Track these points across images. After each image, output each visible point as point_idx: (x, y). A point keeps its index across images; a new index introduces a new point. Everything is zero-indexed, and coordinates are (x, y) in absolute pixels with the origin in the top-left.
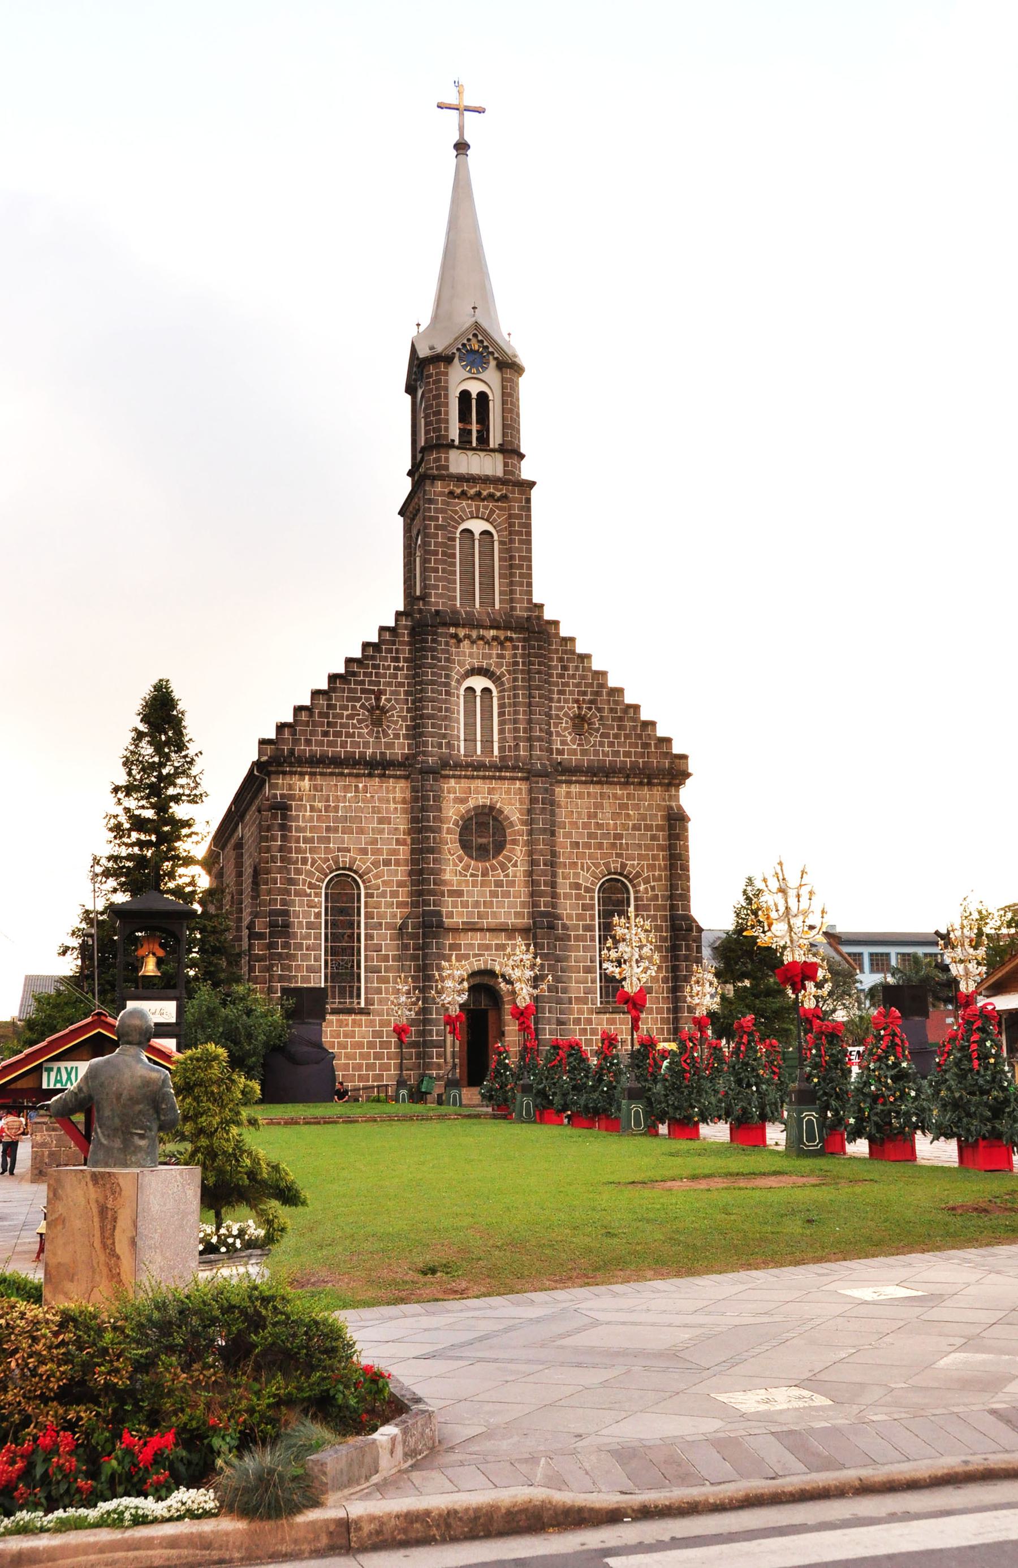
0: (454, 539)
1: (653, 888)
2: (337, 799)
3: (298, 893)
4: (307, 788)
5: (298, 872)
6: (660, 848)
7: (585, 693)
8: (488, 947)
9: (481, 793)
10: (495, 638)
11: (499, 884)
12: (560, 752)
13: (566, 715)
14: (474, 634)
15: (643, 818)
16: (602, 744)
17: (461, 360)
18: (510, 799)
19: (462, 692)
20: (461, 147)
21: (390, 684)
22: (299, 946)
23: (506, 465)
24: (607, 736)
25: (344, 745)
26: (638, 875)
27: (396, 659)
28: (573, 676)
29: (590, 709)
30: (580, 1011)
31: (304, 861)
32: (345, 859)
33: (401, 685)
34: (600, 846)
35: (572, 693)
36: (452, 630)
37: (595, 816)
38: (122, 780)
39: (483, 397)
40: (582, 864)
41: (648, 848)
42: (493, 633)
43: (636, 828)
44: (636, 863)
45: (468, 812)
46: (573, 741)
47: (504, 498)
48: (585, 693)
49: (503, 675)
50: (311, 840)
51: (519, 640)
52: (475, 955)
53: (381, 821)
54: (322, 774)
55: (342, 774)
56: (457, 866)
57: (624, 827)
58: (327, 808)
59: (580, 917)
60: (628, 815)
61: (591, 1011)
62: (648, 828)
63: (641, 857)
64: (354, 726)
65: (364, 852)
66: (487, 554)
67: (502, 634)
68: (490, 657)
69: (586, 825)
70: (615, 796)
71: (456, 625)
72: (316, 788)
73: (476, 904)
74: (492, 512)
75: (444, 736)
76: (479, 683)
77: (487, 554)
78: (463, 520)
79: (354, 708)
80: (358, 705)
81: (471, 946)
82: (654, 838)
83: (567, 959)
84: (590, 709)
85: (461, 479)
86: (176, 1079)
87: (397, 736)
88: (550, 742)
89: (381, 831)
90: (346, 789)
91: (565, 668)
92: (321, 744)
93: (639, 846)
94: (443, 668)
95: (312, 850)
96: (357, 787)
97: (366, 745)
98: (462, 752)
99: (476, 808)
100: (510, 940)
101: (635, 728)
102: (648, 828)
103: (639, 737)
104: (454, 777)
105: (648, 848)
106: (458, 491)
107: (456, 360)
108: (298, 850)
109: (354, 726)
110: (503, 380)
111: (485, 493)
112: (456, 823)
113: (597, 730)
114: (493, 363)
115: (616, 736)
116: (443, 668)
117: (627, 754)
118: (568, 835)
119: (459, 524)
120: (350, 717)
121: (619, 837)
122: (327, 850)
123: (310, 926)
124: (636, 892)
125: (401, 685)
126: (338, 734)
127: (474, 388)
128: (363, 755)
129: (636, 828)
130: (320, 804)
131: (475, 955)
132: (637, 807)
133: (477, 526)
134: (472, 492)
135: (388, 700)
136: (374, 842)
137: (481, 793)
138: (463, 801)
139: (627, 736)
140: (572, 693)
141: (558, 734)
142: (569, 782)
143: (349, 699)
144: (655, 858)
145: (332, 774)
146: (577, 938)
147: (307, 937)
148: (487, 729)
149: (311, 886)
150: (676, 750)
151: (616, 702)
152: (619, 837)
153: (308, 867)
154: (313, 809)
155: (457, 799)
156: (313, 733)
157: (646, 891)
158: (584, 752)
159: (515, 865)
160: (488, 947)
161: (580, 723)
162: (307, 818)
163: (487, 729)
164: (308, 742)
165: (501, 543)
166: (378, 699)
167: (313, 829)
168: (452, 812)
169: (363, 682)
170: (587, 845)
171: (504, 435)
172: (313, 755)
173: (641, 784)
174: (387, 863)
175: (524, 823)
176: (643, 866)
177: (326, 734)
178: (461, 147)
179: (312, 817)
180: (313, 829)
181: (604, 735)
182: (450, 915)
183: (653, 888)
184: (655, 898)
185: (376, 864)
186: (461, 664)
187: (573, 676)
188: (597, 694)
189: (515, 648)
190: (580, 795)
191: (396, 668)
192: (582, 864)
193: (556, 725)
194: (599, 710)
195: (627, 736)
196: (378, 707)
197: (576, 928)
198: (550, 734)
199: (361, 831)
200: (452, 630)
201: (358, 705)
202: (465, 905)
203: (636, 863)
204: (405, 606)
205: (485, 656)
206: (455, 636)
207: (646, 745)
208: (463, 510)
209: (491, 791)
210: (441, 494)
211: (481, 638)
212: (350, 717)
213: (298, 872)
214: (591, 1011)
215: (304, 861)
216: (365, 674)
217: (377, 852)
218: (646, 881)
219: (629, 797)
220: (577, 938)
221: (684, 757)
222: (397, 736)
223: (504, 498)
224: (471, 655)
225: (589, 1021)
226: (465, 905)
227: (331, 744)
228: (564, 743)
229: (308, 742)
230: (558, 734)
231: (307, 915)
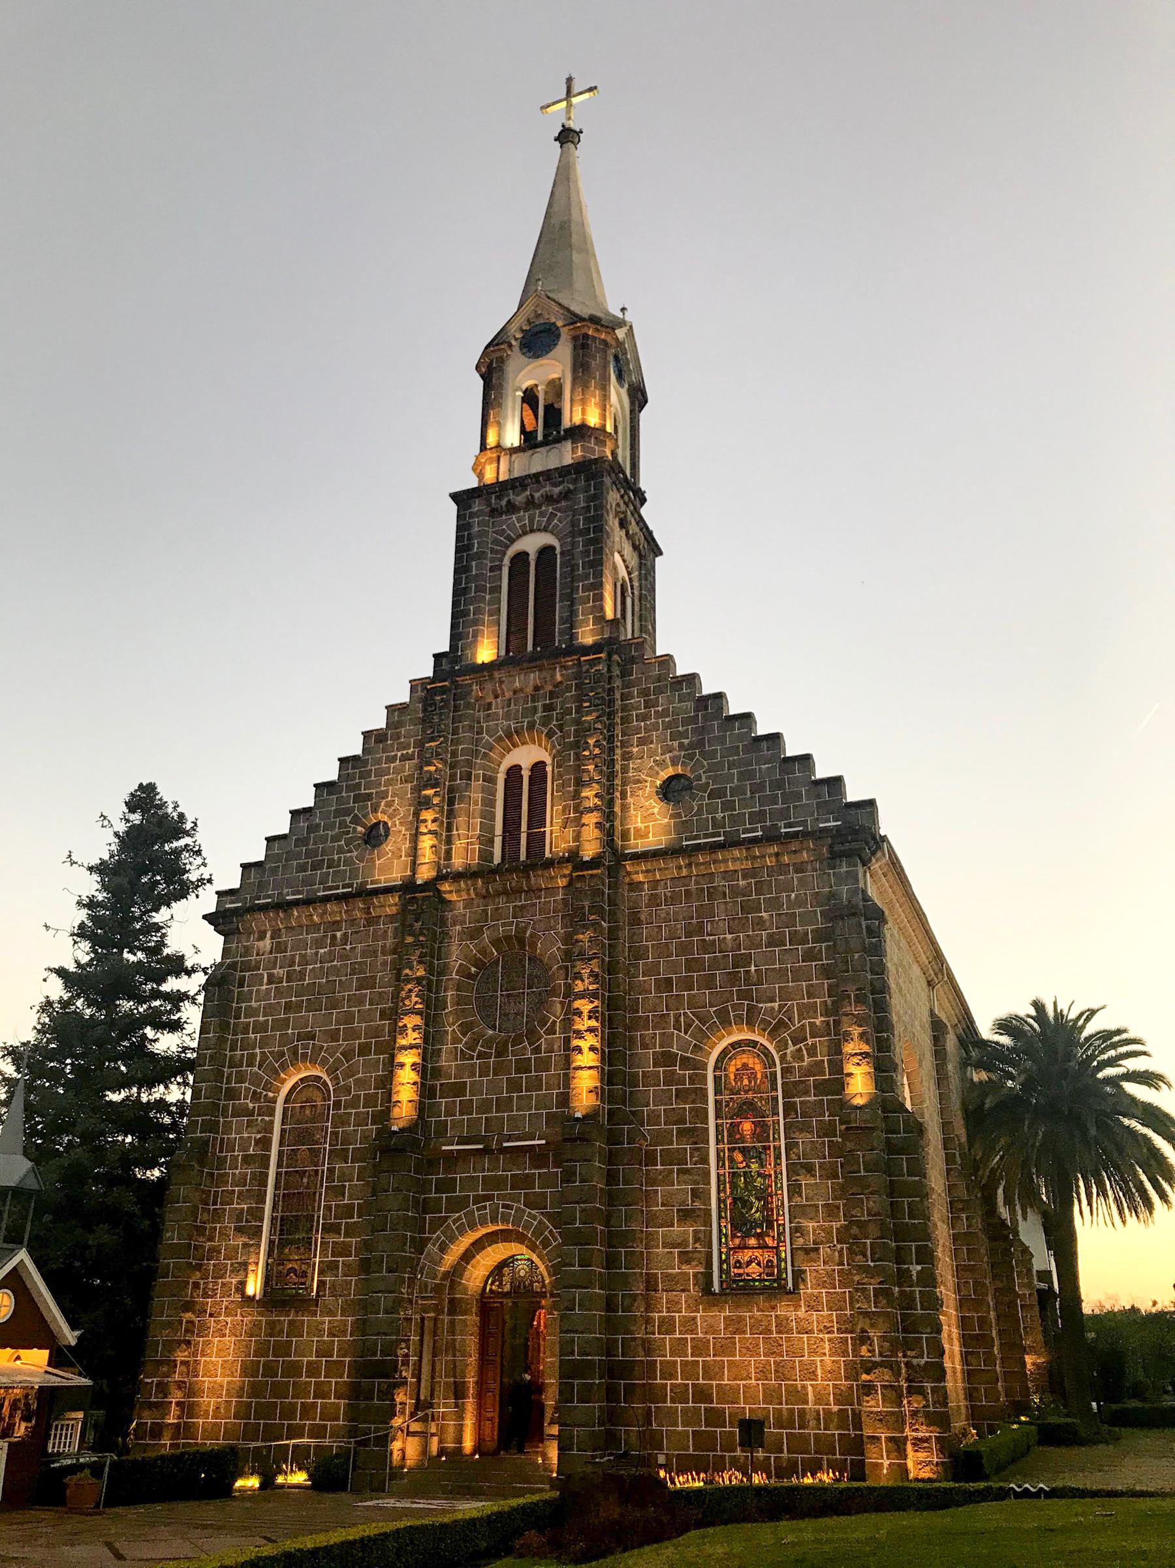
0: (500, 568)
2: (305, 961)
4: (268, 948)
5: (241, 1079)
8: (498, 1183)
11: (523, 1066)
19: (506, 561)
34: (709, 982)
37: (700, 929)
40: (677, 1020)
43: (773, 941)
44: (776, 1005)
52: (478, 1199)
56: (460, 1041)
57: (754, 944)
60: (760, 923)
73: (485, 1106)
78: (512, 541)
79: (343, 824)
80: (348, 819)
82: (809, 956)
83: (649, 1197)
86: (681, 1188)
89: (360, 1001)
93: (782, 973)
96: (334, 937)
100: (537, 1168)
103: (779, 785)
113: (704, 788)
118: (651, 970)
119: (507, 547)
120: (335, 839)
129: (773, 941)
130: (281, 971)
131: (478, 1199)
132: (774, 904)
143: (338, 813)
150: (853, 794)
153: (256, 1069)
159: (551, 1031)
160: (498, 1183)
162: (262, 994)
174: (364, 1050)
176: (791, 1009)
179: (268, 991)
192: (677, 1020)
201: (348, 819)
202: (466, 1108)
203: (776, 1005)
204: (1094, 1318)
208: (511, 526)
209: (520, 911)
212: (335, 839)
217: (352, 1034)
221: (869, 805)
223: (566, 495)
226: (466, 1108)
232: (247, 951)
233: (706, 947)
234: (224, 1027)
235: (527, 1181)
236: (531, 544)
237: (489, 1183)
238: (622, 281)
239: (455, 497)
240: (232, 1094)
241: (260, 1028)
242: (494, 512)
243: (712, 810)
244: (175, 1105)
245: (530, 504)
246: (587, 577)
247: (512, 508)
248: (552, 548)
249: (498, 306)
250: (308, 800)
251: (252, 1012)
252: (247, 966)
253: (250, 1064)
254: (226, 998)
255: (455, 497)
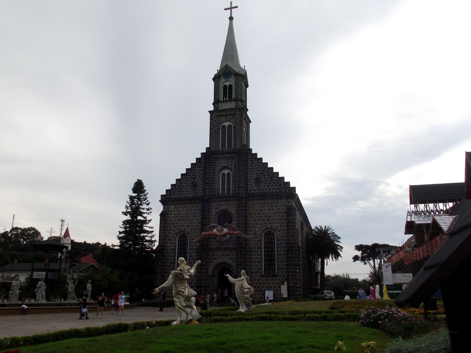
0: (219, 129)
1: (282, 233)
3: (169, 240)
5: (169, 233)
6: (285, 219)
7: (259, 171)
8: (224, 255)
9: (223, 206)
10: (229, 157)
12: (251, 190)
13: (253, 178)
14: (223, 156)
15: (279, 209)
16: (265, 186)
17: (223, 76)
18: (232, 208)
19: (221, 175)
20: (231, 18)
21: (198, 175)
22: (168, 256)
23: (236, 104)
24: (266, 183)
25: (184, 194)
26: (277, 229)
27: (200, 167)
28: (255, 166)
29: (261, 175)
30: (256, 276)
31: (171, 230)
32: (183, 229)
33: (201, 175)
35: (255, 171)
36: (216, 156)
37: (262, 210)
38: (125, 210)
39: (230, 86)
41: (280, 219)
42: (228, 155)
43: (276, 213)
45: (219, 212)
46: (255, 186)
47: (234, 114)
48: (259, 171)
49: (232, 168)
50: (173, 224)
51: (237, 156)
53: (194, 217)
54: (177, 204)
55: (182, 203)
57: (272, 213)
58: (178, 214)
59: (256, 244)
61: (259, 276)
62: (280, 213)
63: (278, 223)
64: (187, 189)
65: (188, 226)
66: (230, 132)
67: (231, 155)
68: (228, 163)
69: (259, 214)
70: (269, 203)
71: (217, 154)
72: (175, 208)
74: (231, 119)
75: (212, 189)
76: (226, 172)
77: (230, 132)
78: (222, 123)
79: (187, 183)
81: (218, 255)
82: (282, 216)
84: (261, 175)
85: (224, 110)
87: (200, 190)
88: (247, 187)
90: (184, 208)
91: (253, 163)
92: (178, 195)
94: (213, 168)
95: (174, 227)
97: (191, 194)
98: (221, 193)
99: (222, 210)
101: (276, 180)
102: (280, 213)
104: (214, 201)
105: (280, 219)
106: (220, 114)
107: (222, 77)
108: (170, 227)
109: (187, 189)
110: (236, 79)
111: (228, 114)
112: (215, 216)
114: (233, 75)
115: (269, 183)
116: (213, 168)
117: (273, 189)
118: (252, 217)
120: (186, 186)
121: (270, 216)
122: (178, 226)
123: (172, 249)
124: (277, 235)
125: (201, 175)
126: (183, 191)
127: (227, 84)
128: (189, 197)
129: (276, 213)
132: (276, 206)
133: (227, 124)
134: (224, 114)
135: (197, 180)
136: (192, 223)
137: (223, 206)
138: (217, 208)
139: (273, 183)
140: (255, 171)
141: (250, 185)
142: (253, 200)
143: (186, 181)
144: (283, 223)
145: (180, 203)
146: (255, 251)
147: (171, 253)
148: (229, 185)
149: (173, 237)
151: (270, 172)
152: (270, 216)
154: (174, 214)
155: (216, 209)
156: (176, 192)
157: (279, 234)
158: (259, 190)
160: (224, 255)
161: (258, 180)
163: (229, 185)
164: (174, 195)
165: (234, 127)
166: (194, 180)
167: (174, 220)
168: (214, 212)
169: (190, 175)
170: (259, 220)
171: (236, 95)
172: (186, 197)
173: (277, 198)
175: (236, 214)
177: (179, 192)
178: (231, 18)
180: (174, 220)
181: (266, 183)
182: (212, 245)
183: (282, 233)
184: (283, 237)
185: (192, 230)
186: (219, 166)
187: (255, 166)
188: (263, 170)
189: (236, 159)
190: (257, 204)
191: (200, 170)
193: (250, 182)
194: (264, 175)
195: (273, 183)
196: (195, 182)
197: (255, 248)
198: (247, 185)
199: (188, 220)
200: (216, 156)
205: (227, 163)
206: (217, 158)
207: (280, 185)
208: (222, 120)
210: (215, 116)
211: (225, 157)
212: (186, 186)
213: (169, 233)
214: (259, 276)
215: (171, 230)
216: (191, 173)
218: (280, 231)
219: (274, 203)
220: (255, 251)
222: (200, 190)
223: (234, 114)
224: (222, 163)
225: (259, 280)
227: (181, 194)
228: (252, 187)
229: (174, 195)
230: (250, 185)
231: (171, 246)
232: (168, 208)
233: (263, 213)
234: (165, 223)
235: (229, 255)
236: (227, 124)
237: (222, 255)
238: (245, 61)
239: (209, 112)
240: (168, 236)
241: (173, 224)
242: (218, 116)
243: (265, 186)
244: (116, 303)
245: (226, 115)
246: (239, 134)
247: (222, 115)
248: (231, 125)
249: (215, 67)
250: (164, 193)
251: (170, 221)
252: (169, 211)
253: (171, 231)
254: (165, 217)
255: (209, 112)
